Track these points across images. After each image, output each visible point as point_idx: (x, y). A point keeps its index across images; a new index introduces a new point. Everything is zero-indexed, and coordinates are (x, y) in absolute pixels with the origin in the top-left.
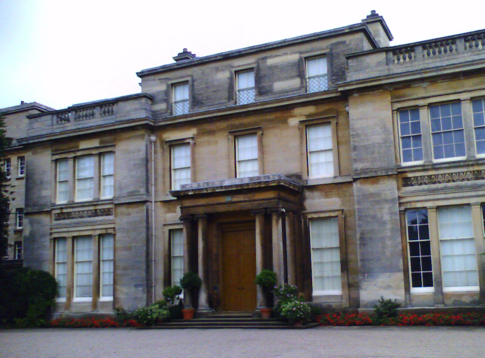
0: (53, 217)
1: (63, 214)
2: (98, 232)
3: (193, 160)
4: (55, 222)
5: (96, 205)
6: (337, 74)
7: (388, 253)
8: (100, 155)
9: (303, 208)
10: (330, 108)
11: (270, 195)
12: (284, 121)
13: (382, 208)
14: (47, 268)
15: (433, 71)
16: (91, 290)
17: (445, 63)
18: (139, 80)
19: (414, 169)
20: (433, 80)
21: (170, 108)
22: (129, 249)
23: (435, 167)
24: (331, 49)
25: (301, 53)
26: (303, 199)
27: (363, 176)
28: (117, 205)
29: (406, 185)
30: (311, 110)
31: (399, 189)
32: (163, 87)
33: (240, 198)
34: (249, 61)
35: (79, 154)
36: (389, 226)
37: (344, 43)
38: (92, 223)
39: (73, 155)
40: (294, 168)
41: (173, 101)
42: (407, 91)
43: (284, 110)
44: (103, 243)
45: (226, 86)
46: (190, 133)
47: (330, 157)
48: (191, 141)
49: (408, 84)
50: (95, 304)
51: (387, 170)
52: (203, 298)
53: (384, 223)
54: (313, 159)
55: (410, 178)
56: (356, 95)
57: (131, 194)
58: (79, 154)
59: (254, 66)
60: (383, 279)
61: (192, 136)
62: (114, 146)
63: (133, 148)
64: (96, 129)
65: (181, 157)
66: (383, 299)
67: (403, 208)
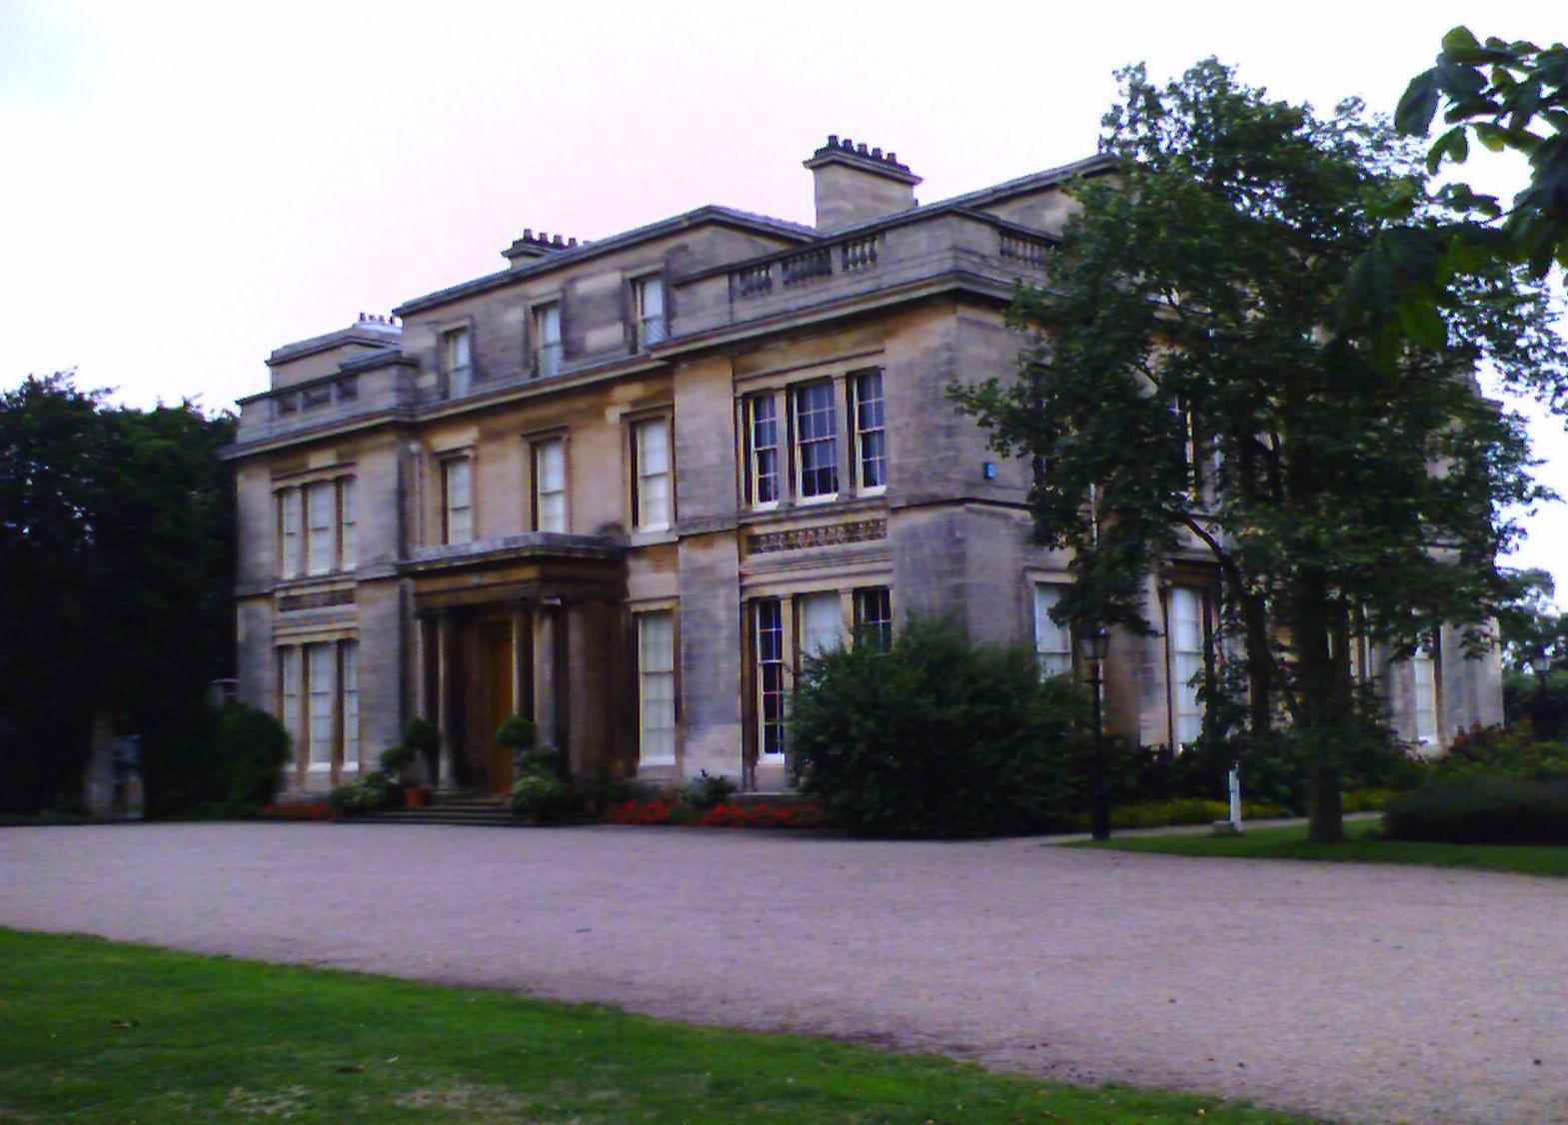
0: (277, 606)
4: (280, 615)
5: (332, 583)
7: (722, 687)
8: (339, 482)
9: (624, 591)
11: (529, 573)
12: (599, 414)
13: (716, 597)
14: (268, 705)
15: (853, 304)
17: (813, 300)
18: (810, 172)
20: (793, 335)
22: (374, 670)
24: (668, 262)
25: (624, 269)
26: (624, 574)
27: (693, 531)
28: (364, 583)
29: (754, 550)
30: (635, 391)
31: (741, 559)
33: (490, 578)
36: (724, 633)
37: (684, 248)
38: (327, 619)
39: (297, 482)
41: (540, 343)
42: (759, 358)
44: (806, 618)
45: (520, 338)
48: (467, 452)
49: (756, 344)
50: (334, 775)
51: (723, 519)
52: (444, 766)
53: (717, 627)
55: (760, 536)
56: (684, 366)
58: (309, 478)
59: (558, 296)
61: (471, 443)
62: (352, 464)
64: (273, 442)
66: (704, 775)
67: (746, 598)
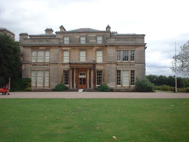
1: (34, 64)
2: (45, 70)
3: (70, 55)
6: (104, 41)
10: (103, 47)
16: (43, 83)
19: (119, 62)
21: (64, 42)
23: (123, 63)
32: (62, 37)
34: (84, 34)
35: (39, 50)
36: (113, 73)
40: (94, 59)
42: (119, 47)
43: (92, 47)
46: (70, 48)
47: (101, 58)
50: (44, 86)
54: (97, 58)
57: (55, 61)
60: (111, 83)
63: (56, 51)
65: (66, 54)
